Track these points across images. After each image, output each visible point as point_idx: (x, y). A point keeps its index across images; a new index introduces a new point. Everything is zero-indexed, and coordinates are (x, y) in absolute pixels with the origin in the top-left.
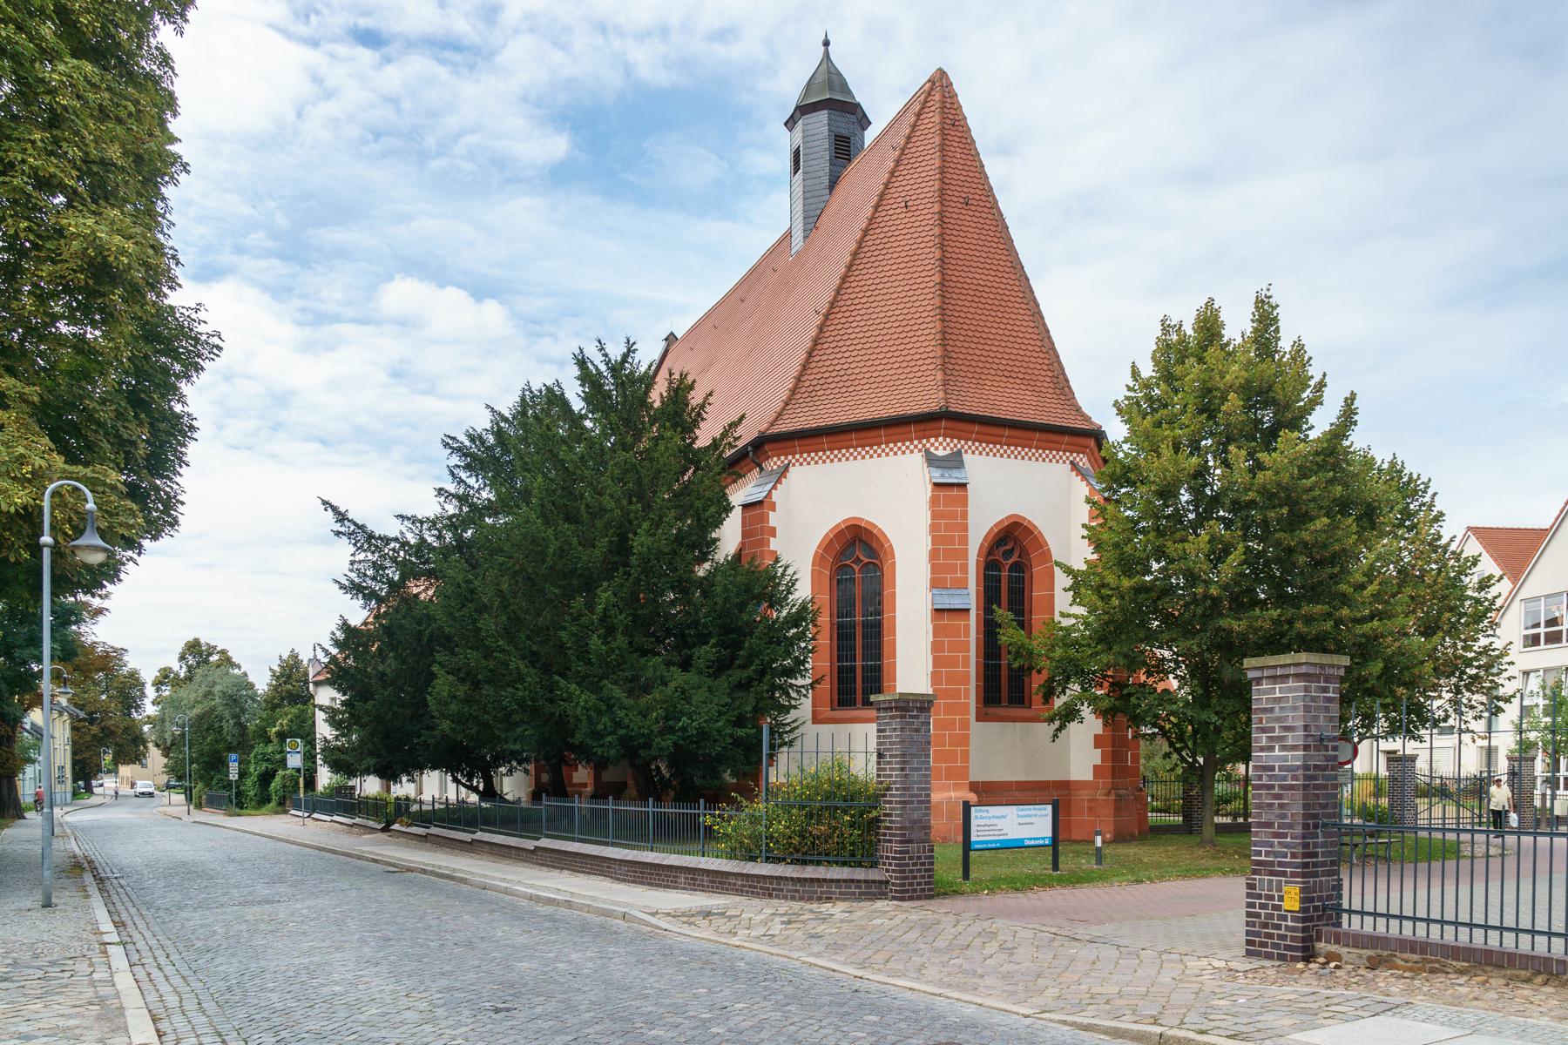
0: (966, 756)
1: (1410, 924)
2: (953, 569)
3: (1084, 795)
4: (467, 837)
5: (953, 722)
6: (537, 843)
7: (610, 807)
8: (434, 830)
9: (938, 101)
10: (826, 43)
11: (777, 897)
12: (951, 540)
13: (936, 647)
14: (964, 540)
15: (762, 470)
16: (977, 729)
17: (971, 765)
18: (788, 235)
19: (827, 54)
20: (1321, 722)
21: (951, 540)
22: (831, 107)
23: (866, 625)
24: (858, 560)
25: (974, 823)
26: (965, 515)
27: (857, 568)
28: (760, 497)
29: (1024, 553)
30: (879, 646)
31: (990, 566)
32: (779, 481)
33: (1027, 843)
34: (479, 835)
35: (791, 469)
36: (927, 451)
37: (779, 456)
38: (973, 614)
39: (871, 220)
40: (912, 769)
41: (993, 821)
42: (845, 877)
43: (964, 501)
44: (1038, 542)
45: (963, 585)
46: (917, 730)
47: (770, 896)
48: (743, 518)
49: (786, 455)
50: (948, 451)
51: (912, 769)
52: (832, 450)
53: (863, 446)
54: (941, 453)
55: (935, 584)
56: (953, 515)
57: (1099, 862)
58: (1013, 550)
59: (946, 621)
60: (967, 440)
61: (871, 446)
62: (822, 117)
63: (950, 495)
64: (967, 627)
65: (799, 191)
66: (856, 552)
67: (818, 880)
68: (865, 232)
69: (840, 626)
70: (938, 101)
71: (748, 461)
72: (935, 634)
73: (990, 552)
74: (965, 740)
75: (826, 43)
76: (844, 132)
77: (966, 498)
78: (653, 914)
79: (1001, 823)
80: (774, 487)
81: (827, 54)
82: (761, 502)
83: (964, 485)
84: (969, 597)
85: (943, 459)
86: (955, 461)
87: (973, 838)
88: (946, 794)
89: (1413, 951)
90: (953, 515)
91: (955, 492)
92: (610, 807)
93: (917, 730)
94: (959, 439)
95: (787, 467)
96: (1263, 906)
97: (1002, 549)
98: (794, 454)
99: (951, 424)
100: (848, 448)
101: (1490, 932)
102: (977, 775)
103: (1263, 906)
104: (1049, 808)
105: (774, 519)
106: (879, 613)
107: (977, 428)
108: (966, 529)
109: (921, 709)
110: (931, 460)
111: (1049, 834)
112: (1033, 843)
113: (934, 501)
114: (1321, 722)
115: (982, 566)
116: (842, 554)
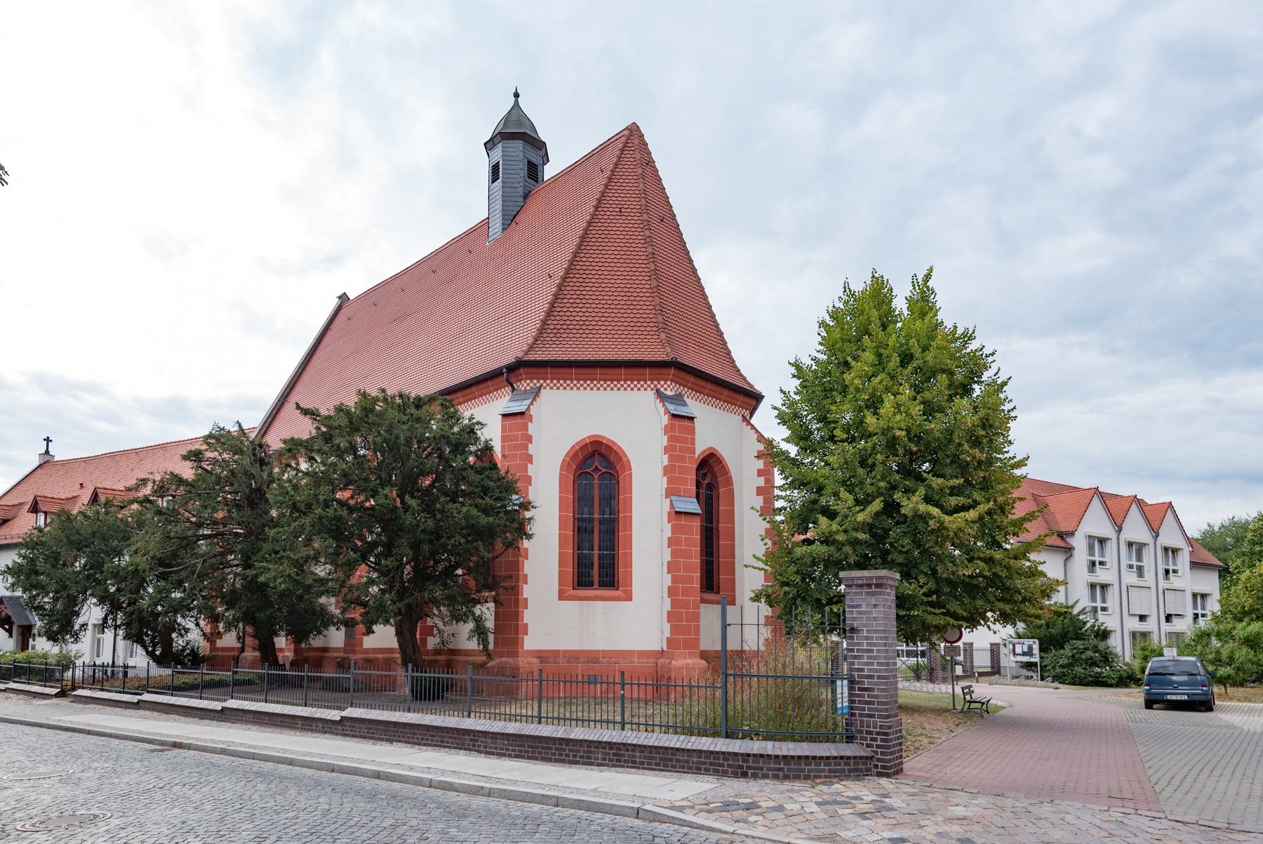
4: (135, 699)
5: (689, 602)
6: (344, 714)
8: (147, 697)
9: (630, 149)
10: (516, 95)
11: (755, 776)
15: (514, 389)
17: (701, 637)
18: (486, 223)
19: (516, 103)
22: (517, 141)
28: (523, 409)
29: (714, 477)
32: (534, 399)
34: (233, 703)
35: (543, 391)
36: (658, 391)
39: (593, 216)
42: (835, 754)
43: (692, 431)
44: (725, 471)
47: (744, 775)
52: (578, 380)
53: (605, 381)
54: (669, 393)
56: (685, 441)
61: (612, 381)
62: (518, 145)
65: (499, 195)
66: (597, 469)
68: (590, 223)
70: (630, 149)
71: (500, 379)
75: (516, 95)
77: (693, 431)
78: (681, 809)
81: (516, 103)
82: (522, 413)
83: (691, 419)
88: (685, 661)
89: (611, 749)
90: (685, 441)
91: (686, 423)
99: (678, 373)
100: (592, 381)
105: (532, 429)
107: (692, 379)
110: (660, 395)
113: (667, 430)
116: (582, 464)
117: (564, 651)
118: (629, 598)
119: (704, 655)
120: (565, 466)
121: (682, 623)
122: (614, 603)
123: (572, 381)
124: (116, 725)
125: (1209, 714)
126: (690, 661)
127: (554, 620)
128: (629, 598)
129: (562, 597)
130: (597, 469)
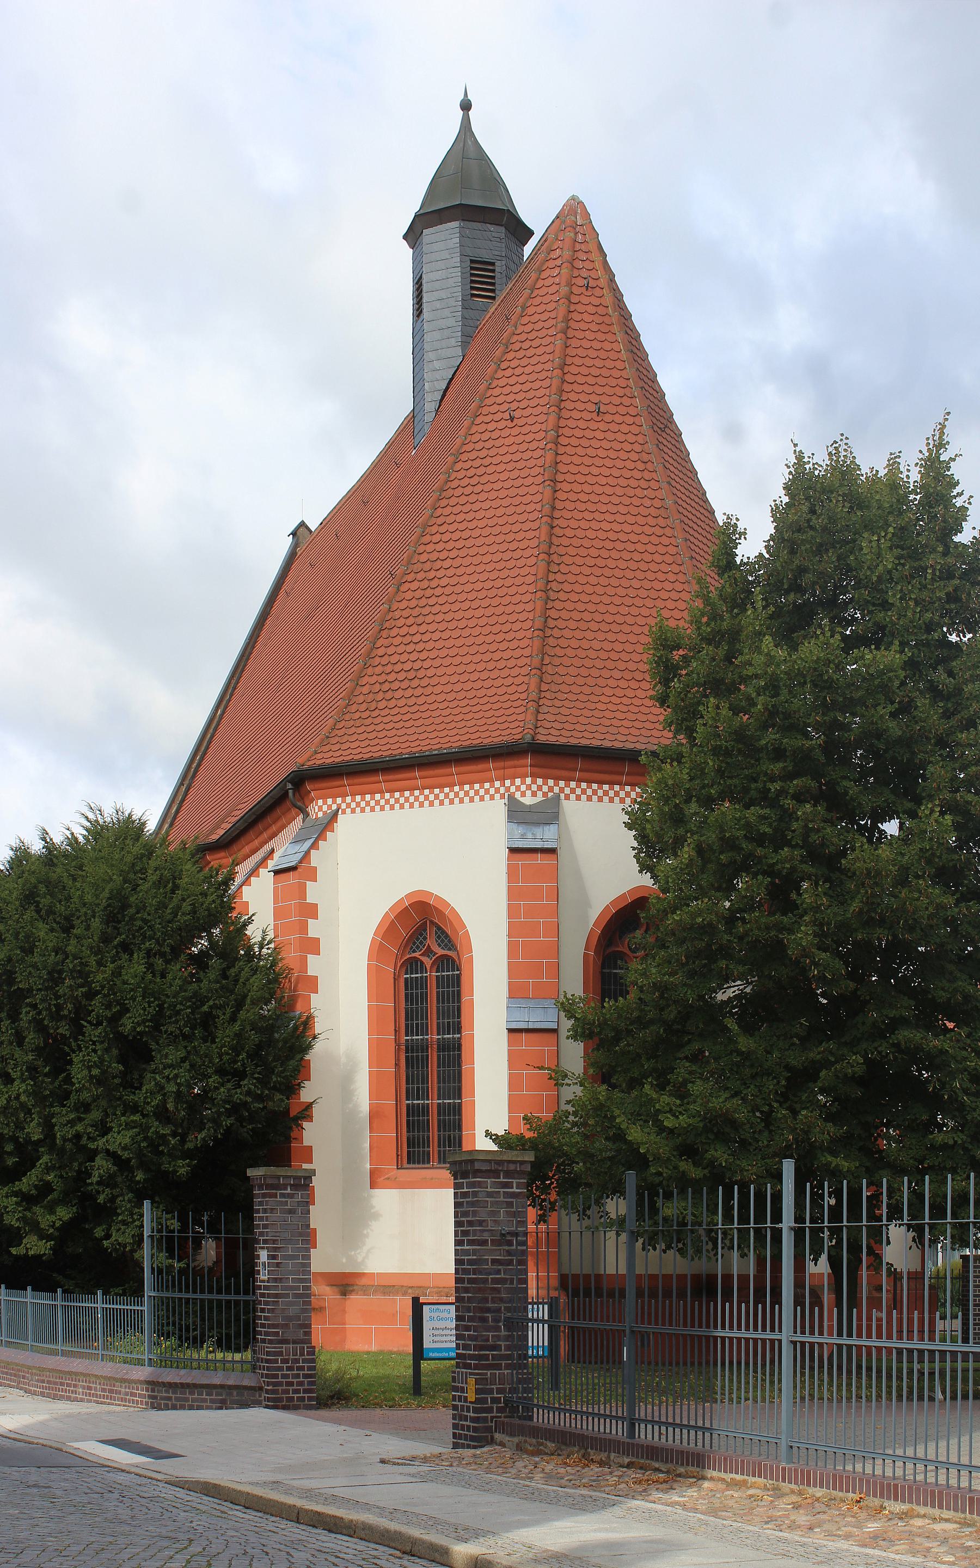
1: (918, 1455)
7: (28, 1300)
10: (466, 106)
19: (466, 125)
20: (502, 1216)
24: (429, 952)
25: (427, 1326)
27: (427, 962)
30: (458, 1077)
32: (321, 836)
35: (340, 817)
36: (511, 798)
37: (325, 798)
40: (284, 1257)
46: (291, 1212)
48: (275, 890)
49: (334, 797)
50: (540, 797)
51: (284, 1257)
54: (528, 800)
63: (535, 864)
67: (187, 1386)
75: (466, 106)
76: (486, 255)
80: (314, 846)
81: (466, 125)
82: (293, 868)
83: (552, 851)
85: (530, 809)
86: (548, 814)
87: (426, 1345)
91: (539, 859)
92: (99, 1305)
93: (291, 1212)
95: (335, 814)
96: (302, 1368)
98: (343, 796)
101: (956, 1461)
103: (302, 1368)
105: (313, 893)
106: (459, 1029)
109: (295, 1187)
110: (516, 813)
113: (512, 873)
114: (502, 1216)
120: (378, 951)
123: (381, 792)
130: (422, 947)
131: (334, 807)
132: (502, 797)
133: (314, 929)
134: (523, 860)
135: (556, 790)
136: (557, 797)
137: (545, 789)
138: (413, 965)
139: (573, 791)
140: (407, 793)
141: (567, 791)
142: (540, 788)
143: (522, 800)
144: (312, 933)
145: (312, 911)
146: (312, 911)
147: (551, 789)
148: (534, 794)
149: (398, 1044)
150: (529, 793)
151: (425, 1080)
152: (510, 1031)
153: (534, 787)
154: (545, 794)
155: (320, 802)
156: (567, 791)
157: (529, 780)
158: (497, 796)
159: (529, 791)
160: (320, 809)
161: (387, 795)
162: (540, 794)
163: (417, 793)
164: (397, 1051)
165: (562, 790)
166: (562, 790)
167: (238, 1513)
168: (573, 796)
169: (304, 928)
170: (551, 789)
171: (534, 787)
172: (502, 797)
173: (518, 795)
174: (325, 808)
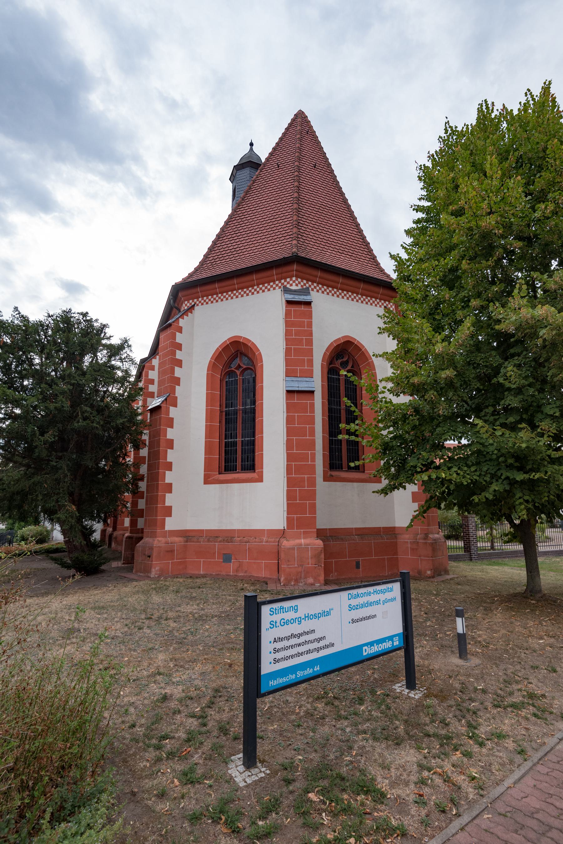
0: (313, 508)
2: (302, 362)
3: (406, 538)
5: (303, 480)
10: (251, 144)
12: (300, 342)
13: (289, 420)
14: (310, 352)
16: (321, 485)
19: (251, 149)
21: (300, 342)
23: (245, 411)
25: (267, 636)
26: (310, 325)
27: (238, 372)
31: (331, 372)
33: (367, 652)
35: (196, 308)
36: (285, 287)
38: (318, 400)
41: (307, 625)
45: (310, 374)
49: (193, 300)
50: (299, 287)
54: (294, 287)
55: (289, 373)
56: (301, 325)
57: (463, 653)
58: (346, 356)
59: (296, 399)
60: (313, 282)
64: (312, 405)
66: (236, 366)
69: (227, 414)
72: (288, 410)
73: (331, 362)
74: (312, 495)
75: (251, 144)
79: (321, 627)
81: (251, 149)
84: (316, 383)
88: (297, 541)
90: (301, 325)
91: (303, 308)
94: (308, 280)
95: (193, 306)
97: (340, 361)
102: (322, 523)
104: (397, 587)
107: (319, 274)
108: (311, 334)
110: (286, 290)
111: (399, 628)
112: (376, 649)
113: (288, 314)
115: (326, 371)
117: (239, 530)
118: (260, 479)
119: (321, 534)
120: (212, 367)
121: (300, 500)
122: (245, 484)
123: (217, 294)
124: (507, 569)
125: (322, 479)
126: (302, 541)
127: (194, 500)
128: (260, 479)
129: (207, 480)
130: (236, 366)
131: (193, 304)
132: (280, 287)
133: (178, 372)
134: (293, 308)
135: (307, 285)
136: (308, 288)
137: (302, 284)
138: (231, 373)
139: (315, 287)
140: (230, 293)
141: (312, 287)
142: (299, 283)
143: (291, 288)
144: (177, 375)
145: (177, 381)
146: (177, 381)
147: (305, 285)
148: (297, 285)
149: (221, 412)
150: (294, 284)
151: (235, 429)
152: (288, 392)
153: (297, 282)
154: (302, 286)
155: (186, 302)
156: (312, 287)
157: (294, 279)
158: (277, 288)
159: (295, 284)
160: (186, 305)
161: (220, 295)
162: (299, 285)
163: (235, 292)
164: (221, 416)
165: (310, 286)
166: (310, 286)
167: (478, 812)
168: (315, 290)
169: (173, 371)
170: (305, 285)
171: (297, 282)
172: (280, 287)
173: (288, 286)
174: (188, 305)
